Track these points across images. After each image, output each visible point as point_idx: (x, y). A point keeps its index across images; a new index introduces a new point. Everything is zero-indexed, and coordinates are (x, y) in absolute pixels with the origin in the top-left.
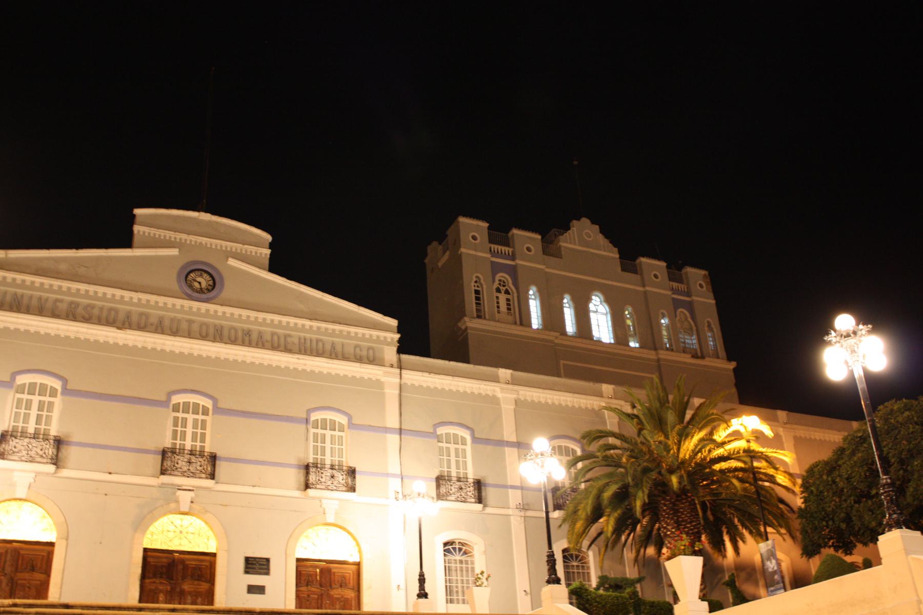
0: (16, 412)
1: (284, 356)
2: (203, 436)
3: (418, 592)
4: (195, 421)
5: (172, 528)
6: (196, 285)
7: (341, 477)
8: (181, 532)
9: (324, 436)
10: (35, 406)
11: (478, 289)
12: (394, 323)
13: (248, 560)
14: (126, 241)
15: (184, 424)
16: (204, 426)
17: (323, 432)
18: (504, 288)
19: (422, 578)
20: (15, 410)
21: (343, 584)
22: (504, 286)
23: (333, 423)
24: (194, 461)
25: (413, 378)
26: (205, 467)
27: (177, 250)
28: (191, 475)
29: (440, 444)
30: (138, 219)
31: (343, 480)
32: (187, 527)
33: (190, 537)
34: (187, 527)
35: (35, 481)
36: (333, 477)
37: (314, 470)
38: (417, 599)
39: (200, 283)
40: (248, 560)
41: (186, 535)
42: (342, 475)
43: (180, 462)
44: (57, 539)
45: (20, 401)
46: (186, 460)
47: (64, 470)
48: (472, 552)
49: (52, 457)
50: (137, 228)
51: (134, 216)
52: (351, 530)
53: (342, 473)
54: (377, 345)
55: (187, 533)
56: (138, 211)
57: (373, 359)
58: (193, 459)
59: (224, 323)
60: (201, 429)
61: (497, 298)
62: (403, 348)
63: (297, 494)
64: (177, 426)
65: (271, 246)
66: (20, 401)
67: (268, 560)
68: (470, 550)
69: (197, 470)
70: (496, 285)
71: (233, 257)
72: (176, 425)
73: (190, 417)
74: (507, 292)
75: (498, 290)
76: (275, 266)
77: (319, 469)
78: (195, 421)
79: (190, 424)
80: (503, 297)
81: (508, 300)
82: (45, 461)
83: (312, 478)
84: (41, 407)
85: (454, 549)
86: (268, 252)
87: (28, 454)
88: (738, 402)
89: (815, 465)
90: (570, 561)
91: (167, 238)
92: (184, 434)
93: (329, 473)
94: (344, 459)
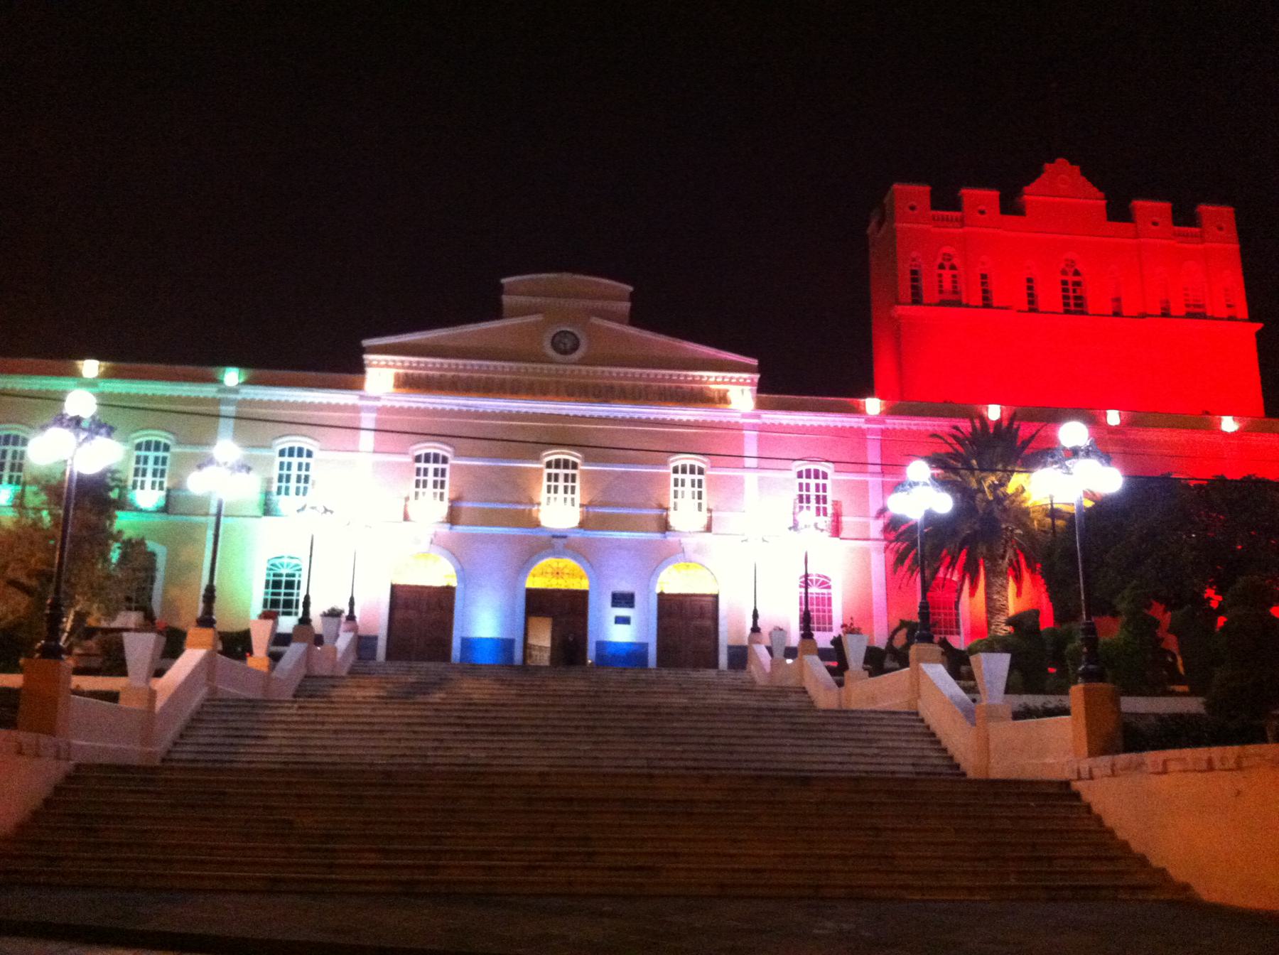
4: (817, 486)
6: (562, 346)
9: (808, 485)
12: (755, 362)
14: (496, 312)
17: (808, 481)
19: (925, 611)
21: (702, 615)
23: (816, 472)
27: (540, 315)
29: (418, 465)
30: (506, 289)
39: (565, 344)
44: (590, 586)
51: (502, 286)
56: (504, 281)
59: (615, 382)
65: (633, 297)
66: (418, 470)
67: (394, 588)
71: (597, 316)
72: (138, 462)
76: (636, 319)
78: (156, 459)
79: (431, 472)
84: (436, 472)
86: (628, 305)
88: (360, 375)
89: (103, 431)
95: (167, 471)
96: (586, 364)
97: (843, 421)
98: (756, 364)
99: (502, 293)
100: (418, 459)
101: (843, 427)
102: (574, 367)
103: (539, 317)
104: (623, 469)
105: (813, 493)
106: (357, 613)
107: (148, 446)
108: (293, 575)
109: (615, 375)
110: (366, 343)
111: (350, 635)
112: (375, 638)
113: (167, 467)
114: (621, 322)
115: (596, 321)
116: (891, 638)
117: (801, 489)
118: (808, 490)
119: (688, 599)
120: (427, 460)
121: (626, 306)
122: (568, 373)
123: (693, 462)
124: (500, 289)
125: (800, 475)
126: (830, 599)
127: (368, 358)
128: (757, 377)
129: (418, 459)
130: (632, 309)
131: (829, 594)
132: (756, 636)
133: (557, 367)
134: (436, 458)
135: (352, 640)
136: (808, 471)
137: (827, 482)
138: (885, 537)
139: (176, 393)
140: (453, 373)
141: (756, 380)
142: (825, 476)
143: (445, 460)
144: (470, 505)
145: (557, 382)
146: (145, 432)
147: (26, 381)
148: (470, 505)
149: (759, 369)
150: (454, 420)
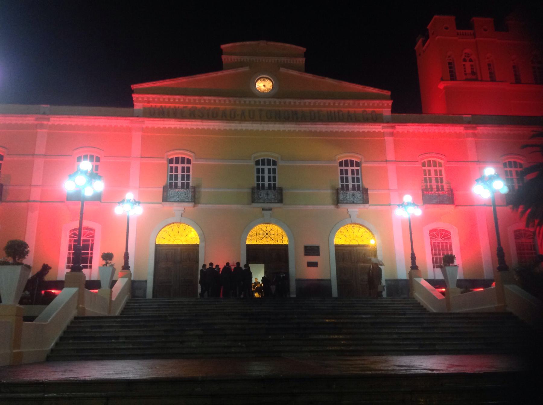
0: (170, 175)
1: (156, 120)
2: (188, 177)
3: (123, 264)
5: (261, 232)
7: (359, 195)
8: (267, 234)
10: (266, 171)
11: (451, 61)
12: (388, 93)
13: (306, 247)
14: (218, 66)
15: (347, 173)
16: (188, 171)
18: (469, 58)
20: (360, 176)
22: (468, 57)
24: (269, 193)
25: (400, 128)
26: (277, 196)
28: (269, 201)
29: (424, 168)
31: (360, 196)
32: (270, 231)
33: (272, 236)
34: (270, 231)
35: (184, 212)
36: (353, 195)
37: (342, 192)
38: (458, 265)
40: (306, 247)
41: (270, 235)
42: (360, 193)
43: (262, 194)
45: (172, 168)
46: (265, 193)
47: (200, 205)
48: (449, 235)
49: (192, 198)
50: (223, 57)
51: (221, 50)
52: (368, 227)
53: (360, 192)
54: (378, 109)
55: (270, 234)
56: (223, 47)
57: (376, 119)
58: (269, 192)
60: (345, 175)
61: (464, 65)
62: (395, 110)
63: (332, 207)
64: (184, 172)
65: (306, 55)
66: (172, 168)
67: (318, 247)
68: (449, 234)
69: (272, 198)
70: (463, 57)
73: (266, 168)
74: (471, 60)
75: (465, 60)
76: (309, 68)
77: (345, 191)
78: (269, 170)
79: (266, 171)
80: (468, 64)
81: (472, 66)
82: (276, 201)
83: (341, 197)
85: (437, 234)
86: (304, 59)
87: (178, 198)
90: (437, 238)
91: (245, 60)
92: (263, 178)
93: (351, 192)
94: (360, 184)
95: (191, 176)
96: (278, 98)
97: (197, 125)
98: (390, 94)
99: (222, 54)
100: (424, 165)
101: (180, 128)
102: (270, 100)
103: (246, 69)
104: (370, 165)
105: (180, 173)
106: (131, 263)
107: (177, 161)
108: (88, 241)
109: (207, 101)
110: (134, 87)
111: (126, 280)
112: (330, 280)
113: (191, 173)
114: (299, 70)
115: (283, 70)
116: (232, 266)
117: (171, 171)
118: (430, 174)
119: (355, 248)
120: (177, 162)
121: (302, 61)
122: (322, 104)
123: (435, 159)
124: (221, 52)
125: (424, 165)
126: (451, 246)
127: (135, 96)
128: (390, 103)
129: (171, 161)
130: (306, 61)
131: (450, 243)
132: (414, 271)
133: (259, 99)
134: (183, 161)
135: (127, 282)
136: (346, 161)
137: (443, 169)
138: (414, 203)
139: (156, 126)
140: (201, 106)
141: (390, 104)
142: (189, 162)
143: (189, 162)
144: (207, 190)
145: (261, 110)
146: (435, 155)
147: (361, 126)
148: (207, 190)
149: (392, 97)
150: (213, 136)
